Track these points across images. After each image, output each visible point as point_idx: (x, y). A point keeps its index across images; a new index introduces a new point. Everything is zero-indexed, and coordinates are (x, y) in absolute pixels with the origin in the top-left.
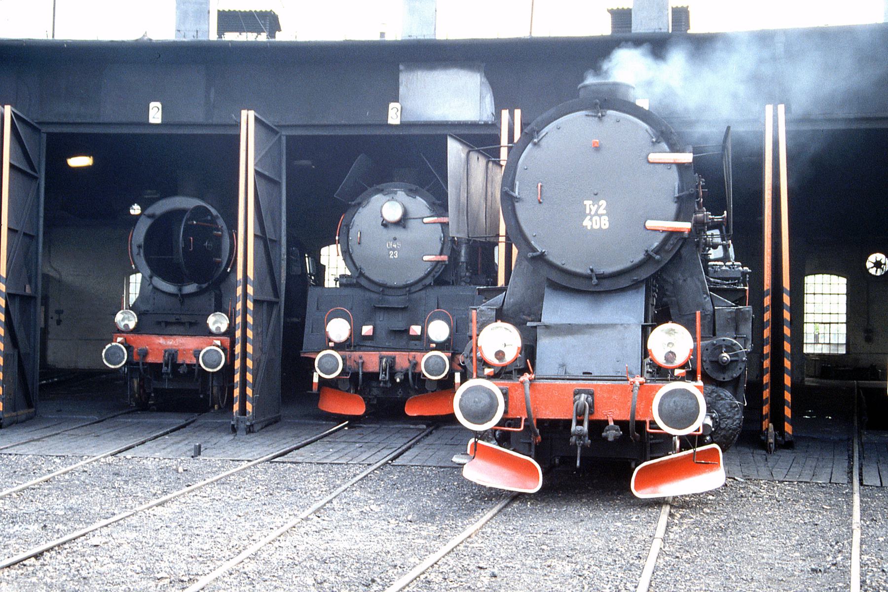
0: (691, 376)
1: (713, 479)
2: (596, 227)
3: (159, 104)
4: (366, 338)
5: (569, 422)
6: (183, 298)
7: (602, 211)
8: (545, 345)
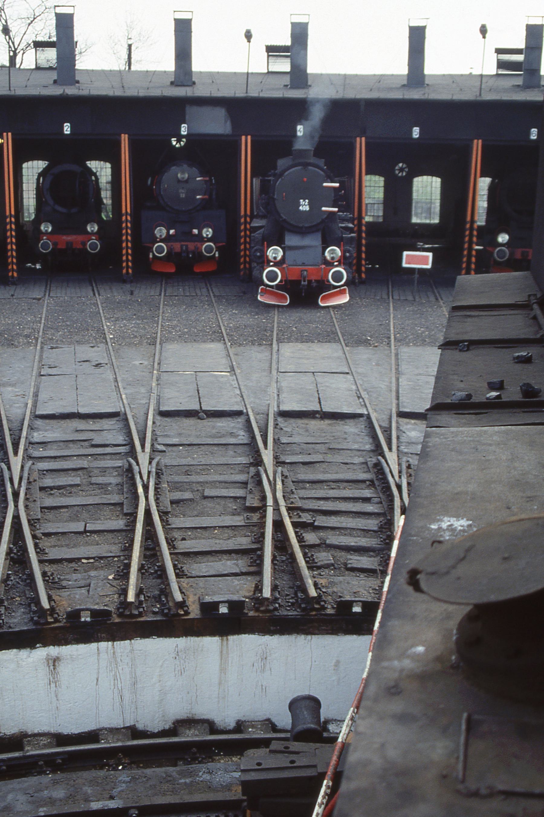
1: (345, 299)
2: (304, 209)
3: (69, 124)
4: (172, 235)
5: (300, 281)
7: (306, 204)
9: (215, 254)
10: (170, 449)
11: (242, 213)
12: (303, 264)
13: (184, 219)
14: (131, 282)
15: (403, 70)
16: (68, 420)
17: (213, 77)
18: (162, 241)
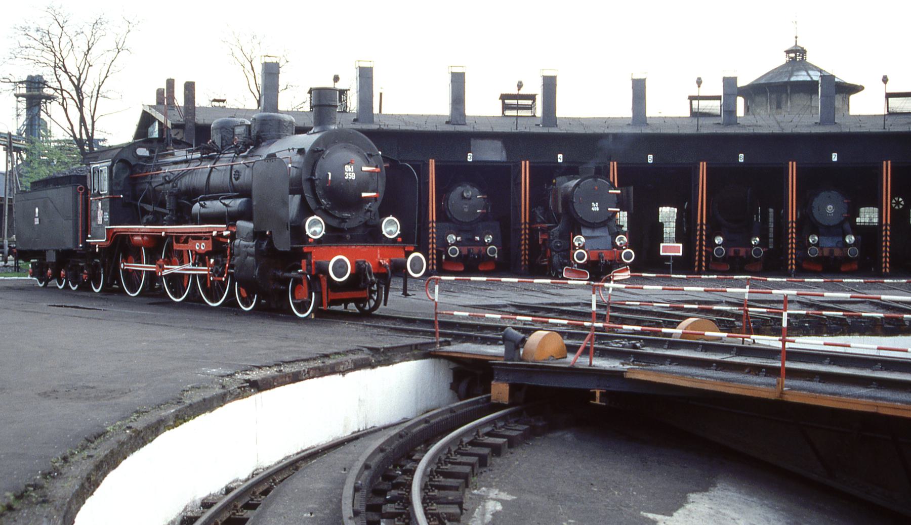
11: (523, 221)
15: (629, 114)
17: (476, 119)
18: (453, 245)
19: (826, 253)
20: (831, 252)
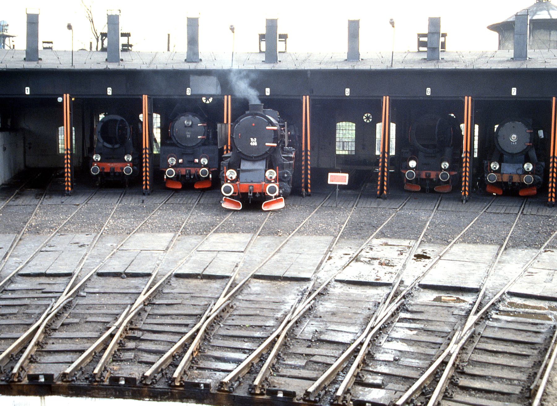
0: (276, 182)
1: (281, 205)
4: (181, 163)
5: (248, 193)
6: (113, 149)
8: (241, 174)
9: (209, 175)
10: (90, 295)
12: (252, 182)
13: (188, 152)
14: (149, 194)
16: (38, 278)
18: (172, 167)
19: (505, 179)
20: (511, 178)
